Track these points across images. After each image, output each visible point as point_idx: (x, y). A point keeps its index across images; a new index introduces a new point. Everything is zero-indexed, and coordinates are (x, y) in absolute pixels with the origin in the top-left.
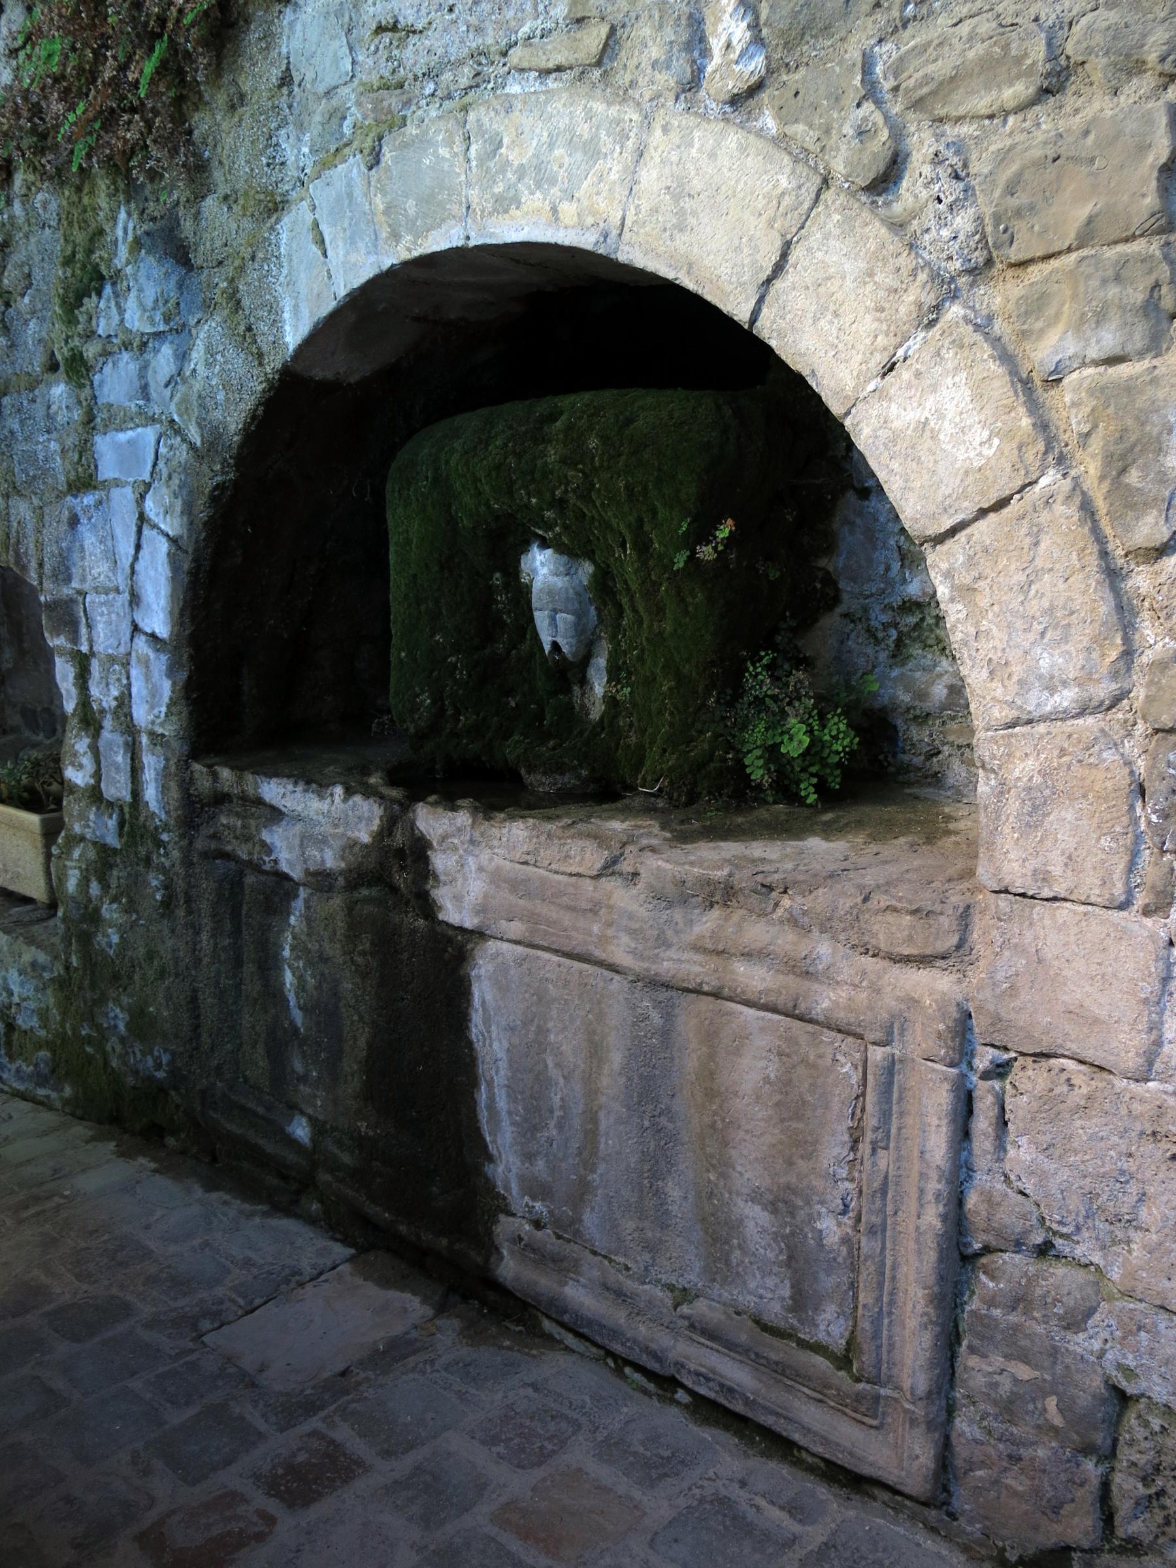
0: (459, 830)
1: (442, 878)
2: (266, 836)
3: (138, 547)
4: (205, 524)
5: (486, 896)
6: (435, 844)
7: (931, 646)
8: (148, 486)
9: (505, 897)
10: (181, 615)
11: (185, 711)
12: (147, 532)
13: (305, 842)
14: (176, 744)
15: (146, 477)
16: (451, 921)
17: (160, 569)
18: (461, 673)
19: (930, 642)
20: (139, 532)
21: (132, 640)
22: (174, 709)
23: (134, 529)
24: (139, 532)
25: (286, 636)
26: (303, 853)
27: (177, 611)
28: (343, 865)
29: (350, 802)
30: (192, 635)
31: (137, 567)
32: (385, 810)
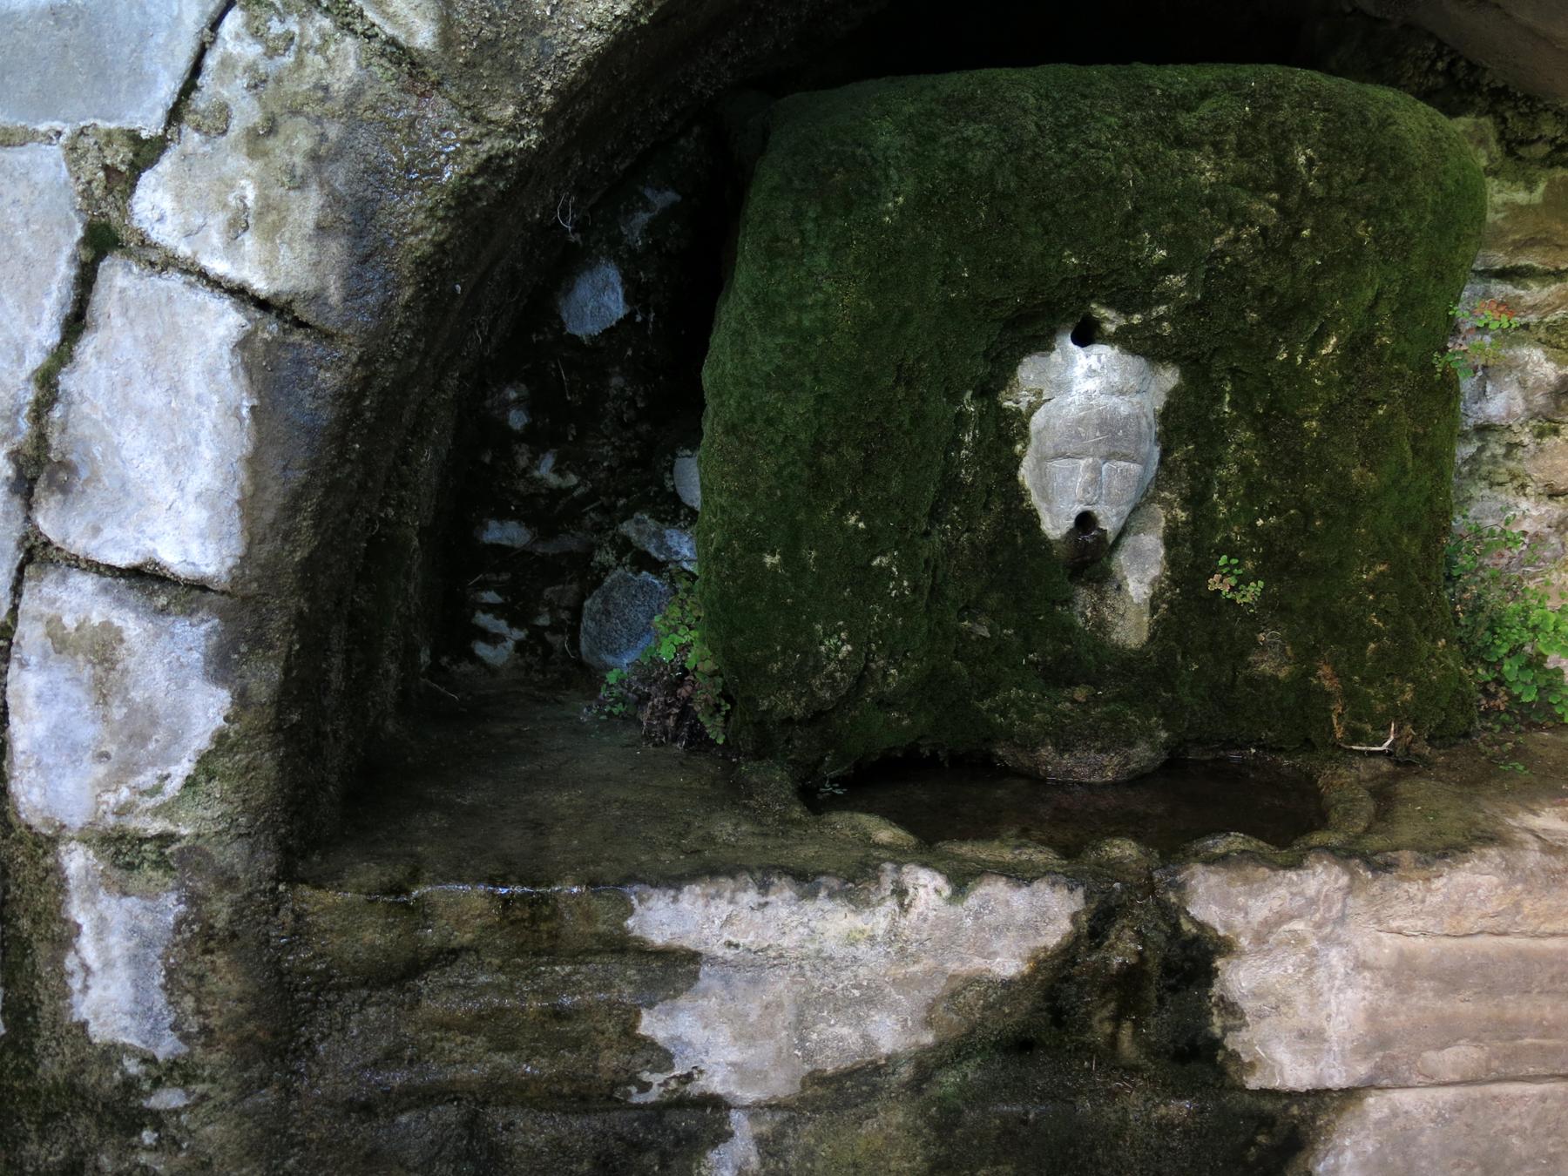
0: (1312, 902)
1: (1248, 1005)
2: (652, 1025)
3: (76, 323)
4: (420, 263)
5: (1373, 1015)
6: (1244, 942)
7: (1501, 484)
8: (146, 152)
9: (1427, 1001)
10: (292, 507)
11: (268, 763)
12: (117, 277)
13: (811, 1013)
14: (230, 855)
15: (150, 124)
16: (1291, 1084)
17: (194, 382)
18: (899, 586)
19: (1501, 479)
20: (86, 279)
21: (17, 590)
22: (222, 764)
23: (64, 270)
24: (86, 279)
25: (1382, 568)
26: (802, 1039)
27: (275, 495)
28: (928, 1038)
29: (972, 901)
30: (309, 564)
31: (68, 381)
32: (1088, 897)
